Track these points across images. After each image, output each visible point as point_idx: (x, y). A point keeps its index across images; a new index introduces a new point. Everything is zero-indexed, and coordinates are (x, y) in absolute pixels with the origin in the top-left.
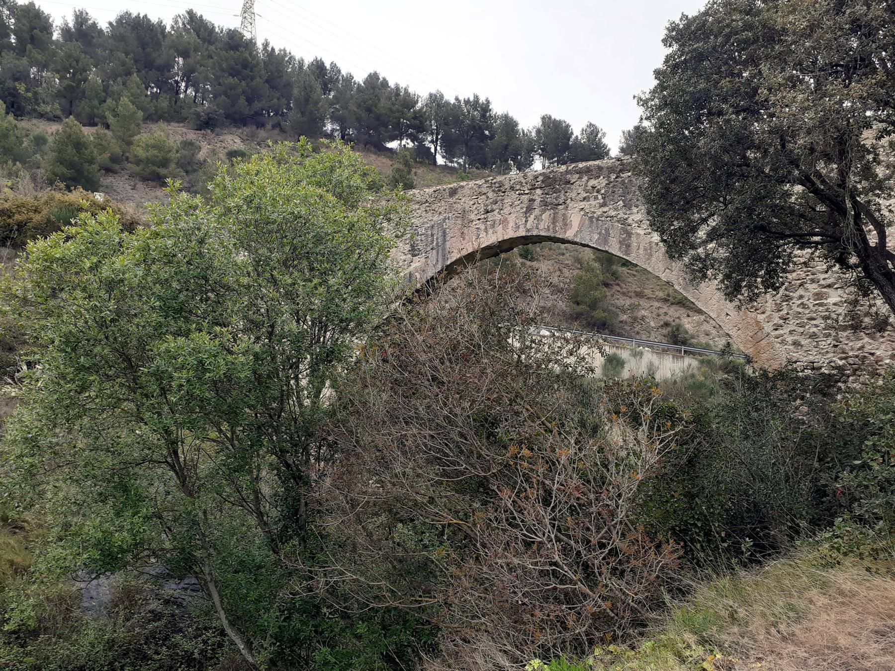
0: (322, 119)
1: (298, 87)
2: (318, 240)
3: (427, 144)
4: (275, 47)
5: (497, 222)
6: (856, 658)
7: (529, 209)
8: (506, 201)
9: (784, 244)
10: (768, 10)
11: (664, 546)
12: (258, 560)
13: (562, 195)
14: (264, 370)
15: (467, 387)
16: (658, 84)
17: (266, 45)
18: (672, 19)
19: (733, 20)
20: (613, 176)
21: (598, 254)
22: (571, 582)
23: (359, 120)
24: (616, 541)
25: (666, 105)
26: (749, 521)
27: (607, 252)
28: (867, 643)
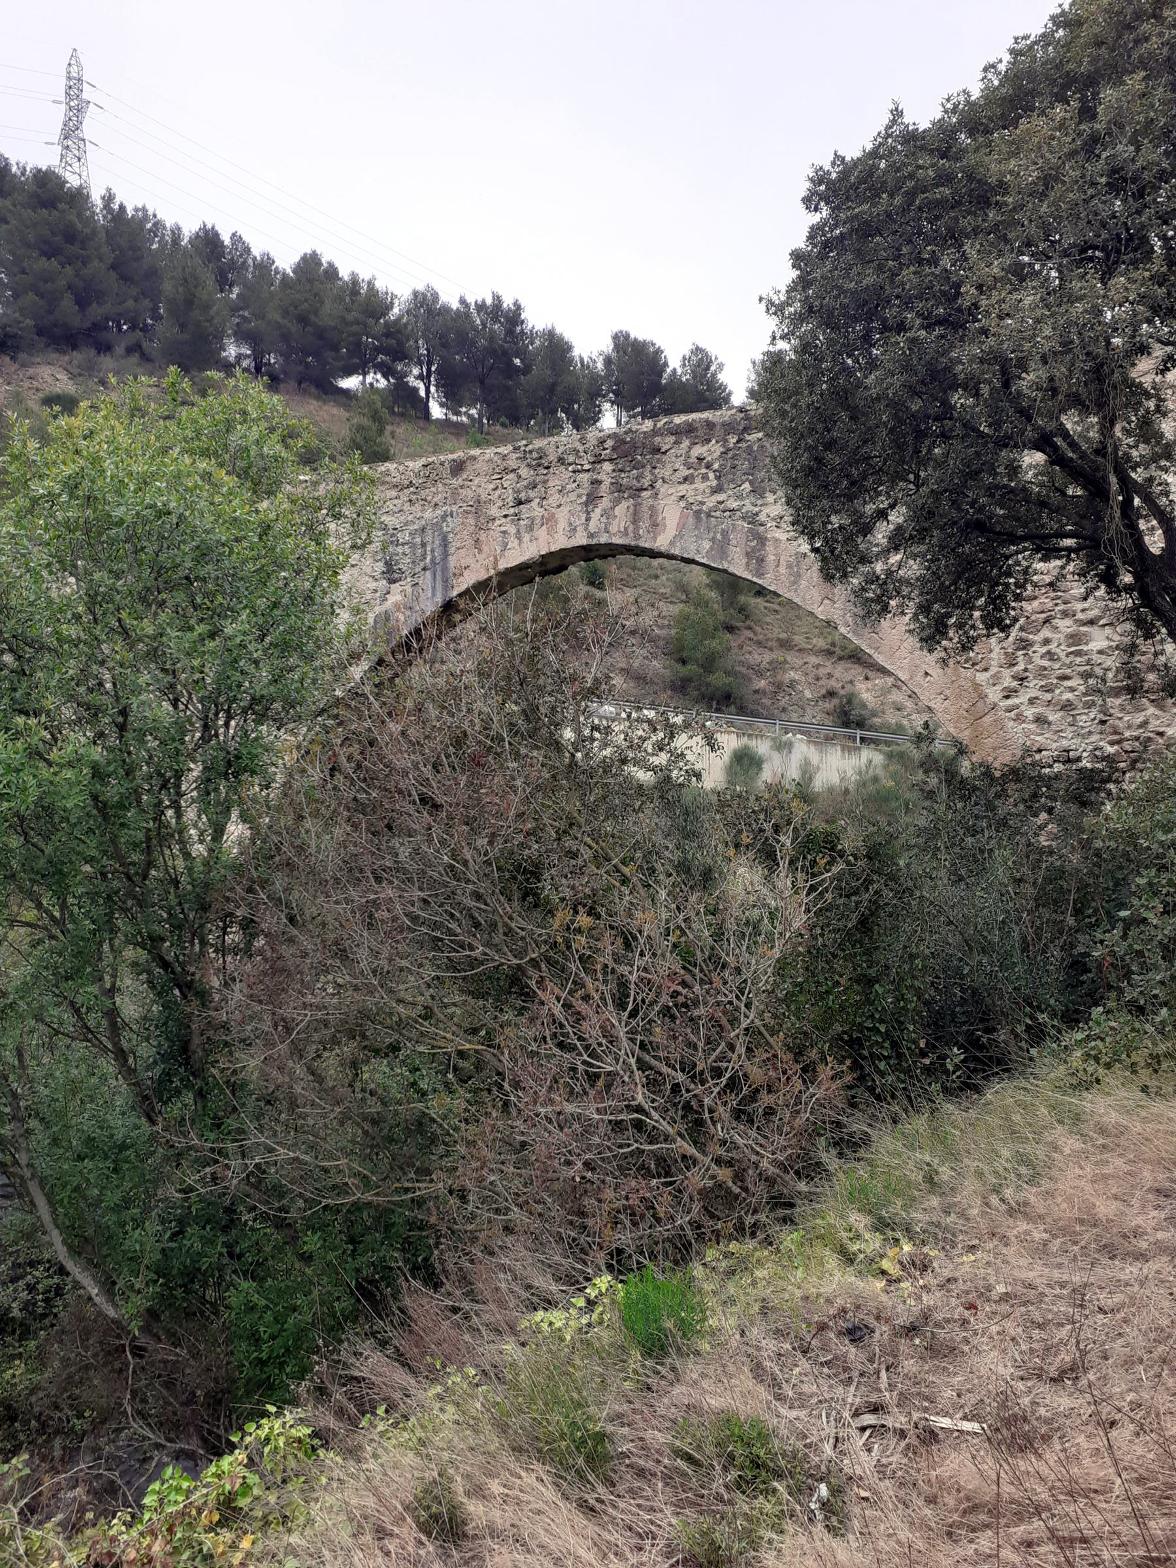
0: (219, 337)
1: (172, 278)
2: (203, 554)
3: (412, 381)
4: (126, 203)
5: (538, 521)
6: (1125, 1236)
7: (592, 499)
8: (551, 484)
9: (1017, 553)
10: (977, 150)
11: (820, 1067)
12: (119, 1136)
13: (647, 473)
14: (113, 790)
15: (482, 812)
16: (799, 277)
17: (109, 199)
18: (819, 162)
19: (920, 167)
20: (733, 440)
21: (715, 576)
22: (667, 1139)
23: (285, 337)
24: (737, 1062)
25: (811, 310)
26: (964, 1019)
27: (725, 571)
28: (1143, 1210)
